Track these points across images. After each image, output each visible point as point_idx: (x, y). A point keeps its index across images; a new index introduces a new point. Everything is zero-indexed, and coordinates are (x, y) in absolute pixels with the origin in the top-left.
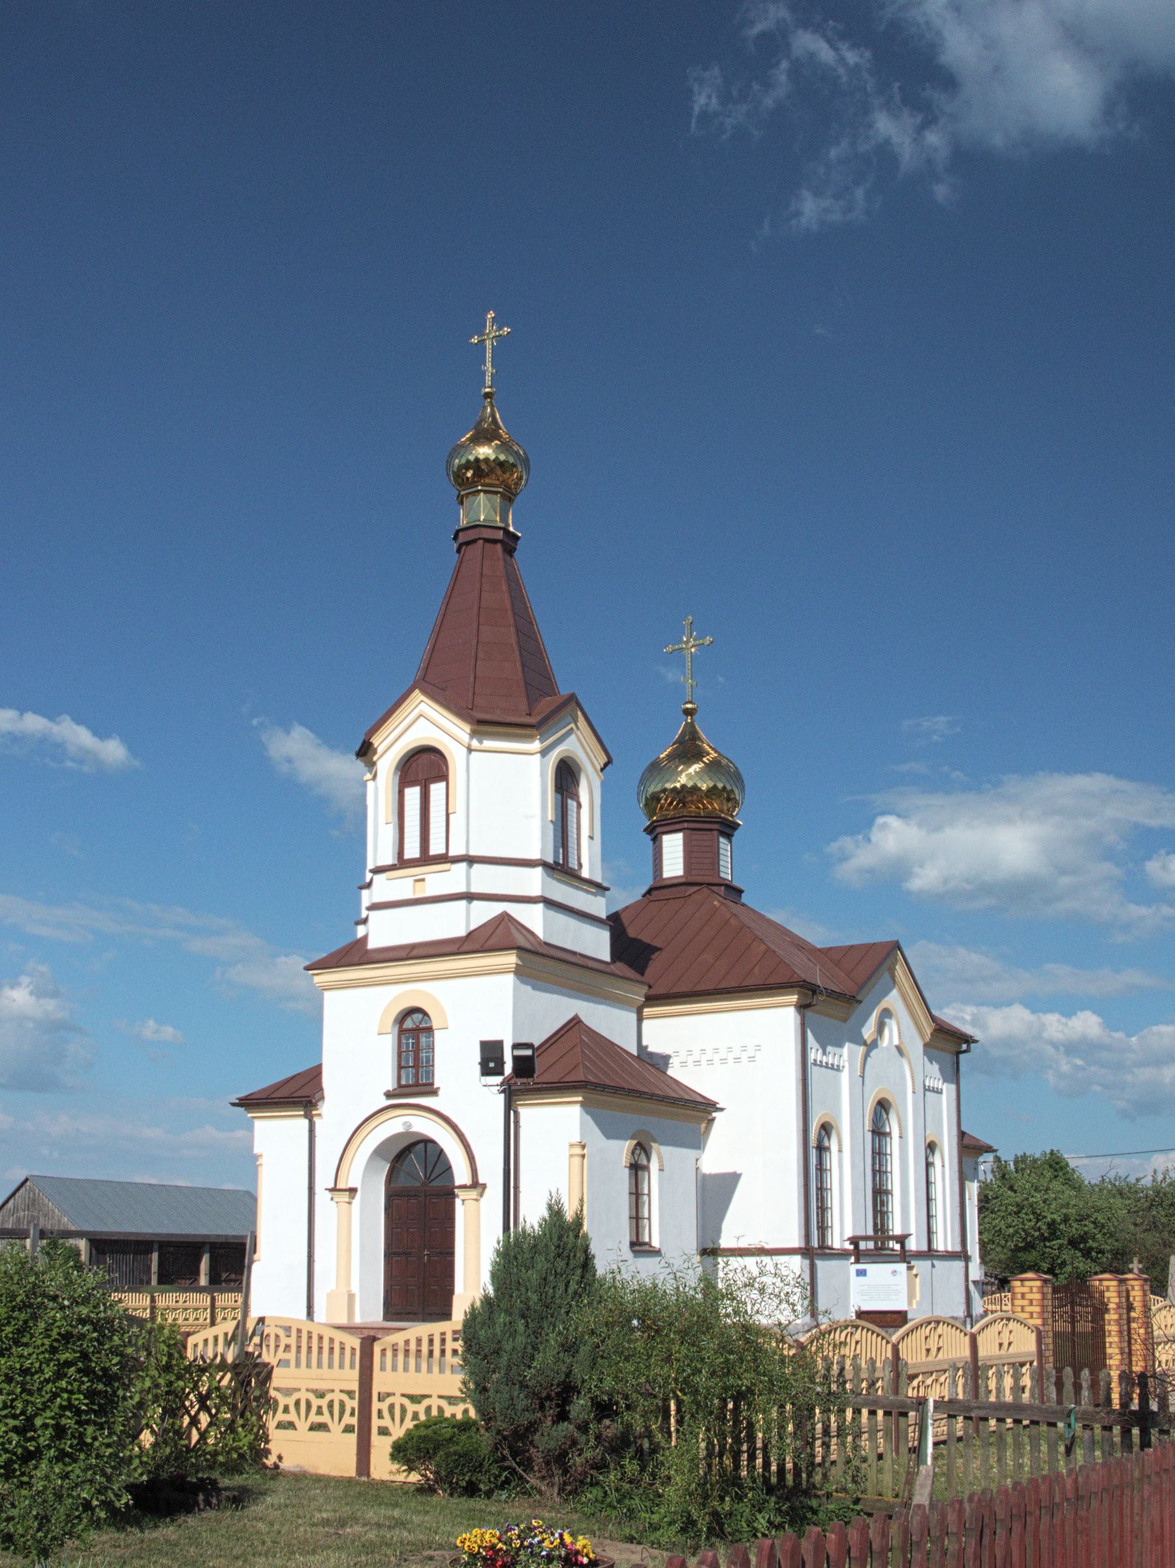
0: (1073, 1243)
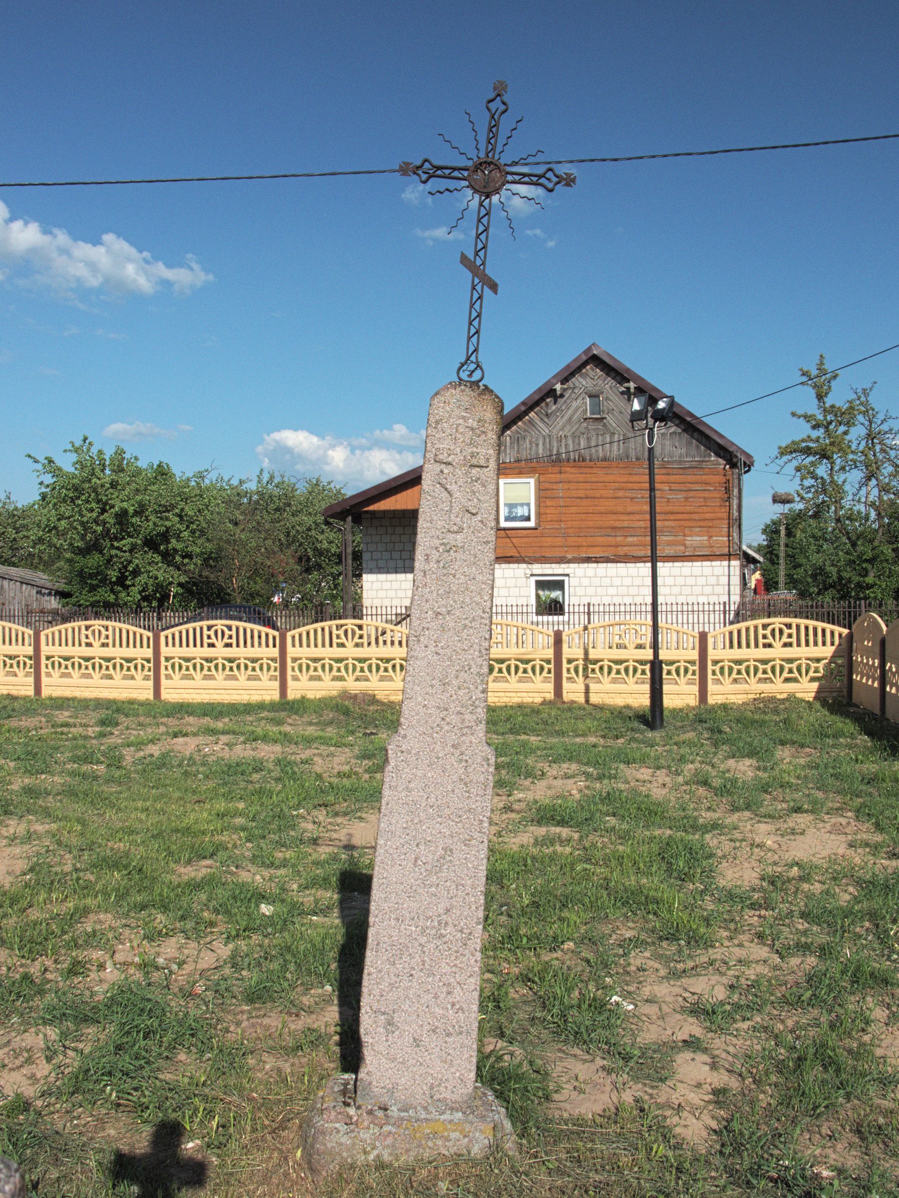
0: (151, 543)
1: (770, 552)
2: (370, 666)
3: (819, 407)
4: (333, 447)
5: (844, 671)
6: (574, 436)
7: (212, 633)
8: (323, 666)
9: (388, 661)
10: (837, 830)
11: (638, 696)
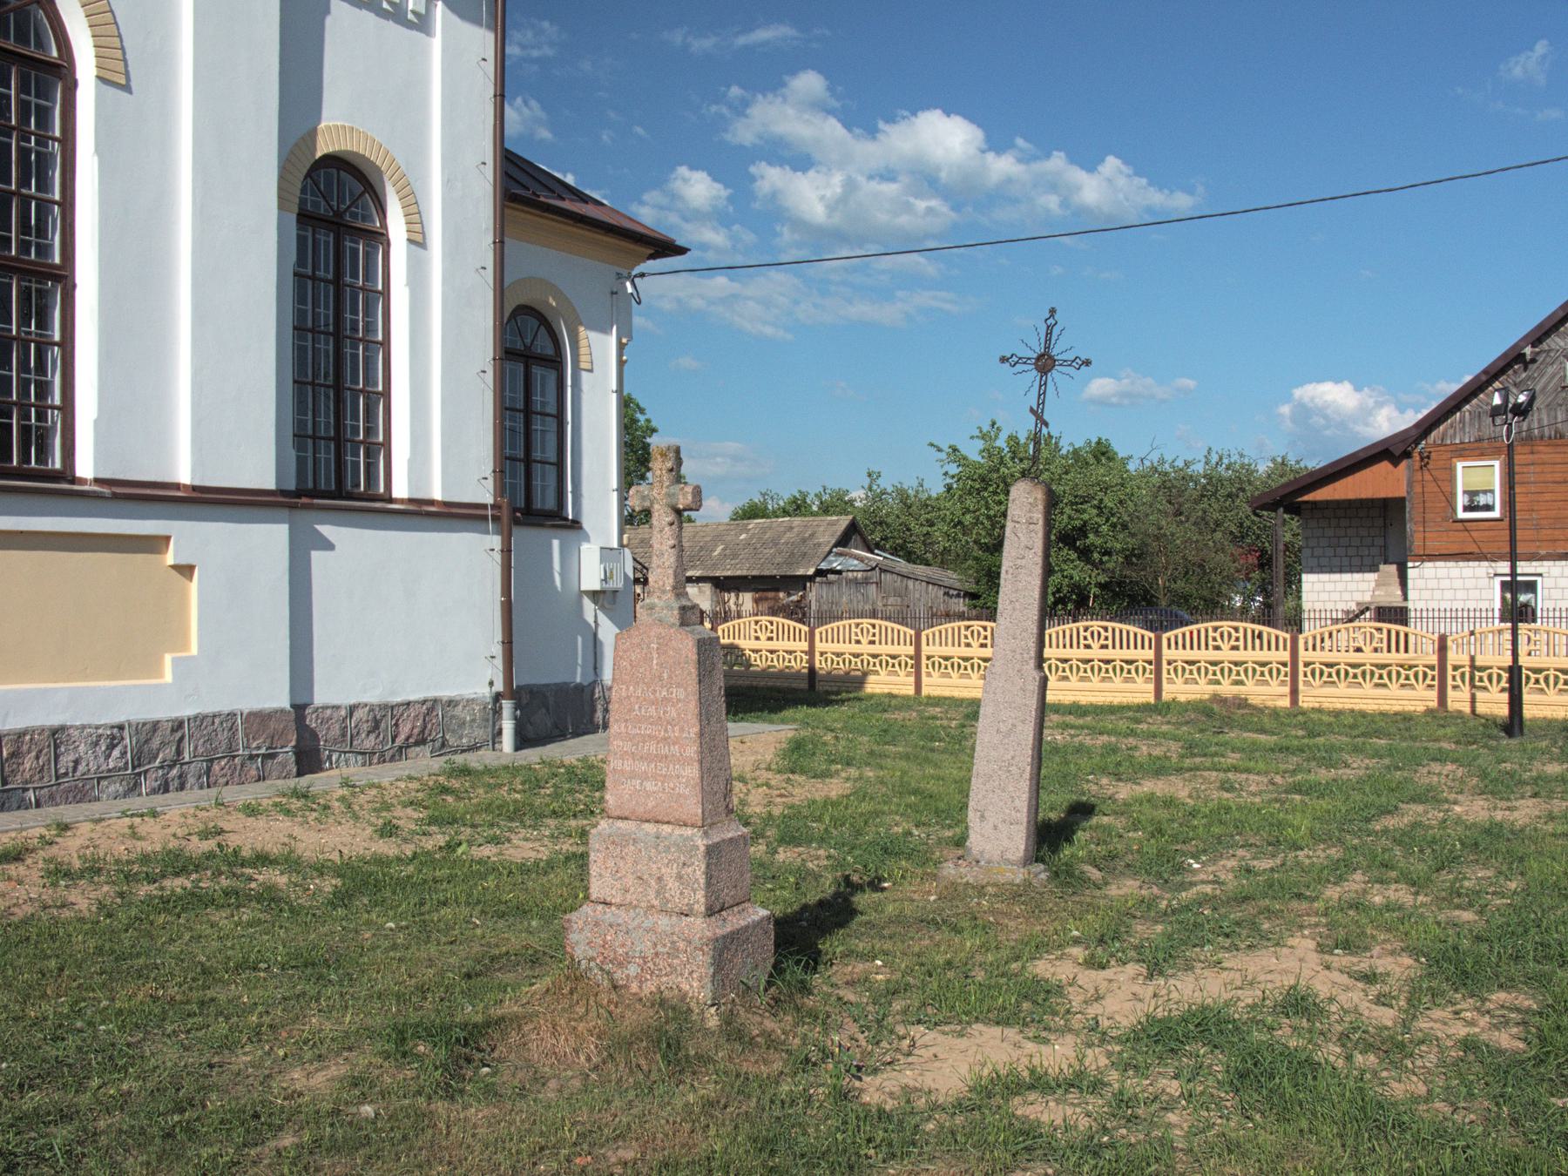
2: (1364, 673)
7: (1217, 635)
8: (1222, 670)
9: (1066, 661)
11: (1495, 703)
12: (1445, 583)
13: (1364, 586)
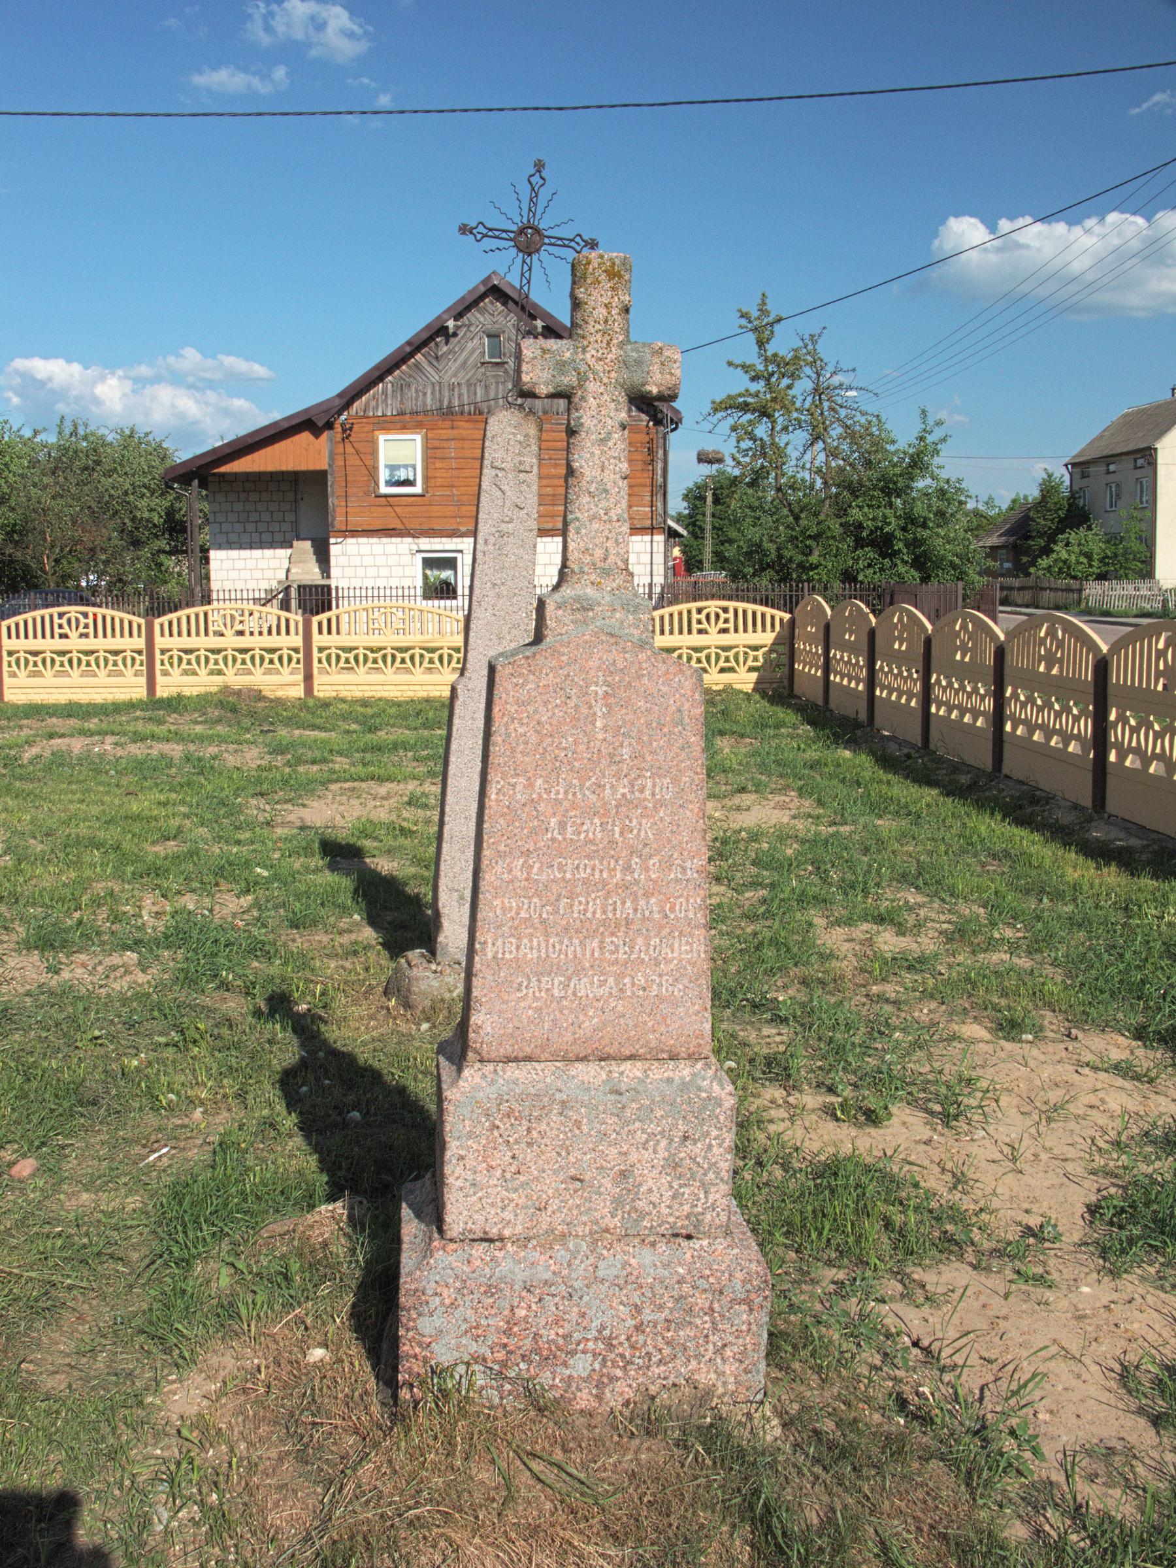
1: (692, 522)
3: (760, 355)
4: (103, 379)
5: (784, 659)
6: (469, 384)
7: (64, 621)
10: (782, 807)
12: (368, 560)
13: (275, 563)
